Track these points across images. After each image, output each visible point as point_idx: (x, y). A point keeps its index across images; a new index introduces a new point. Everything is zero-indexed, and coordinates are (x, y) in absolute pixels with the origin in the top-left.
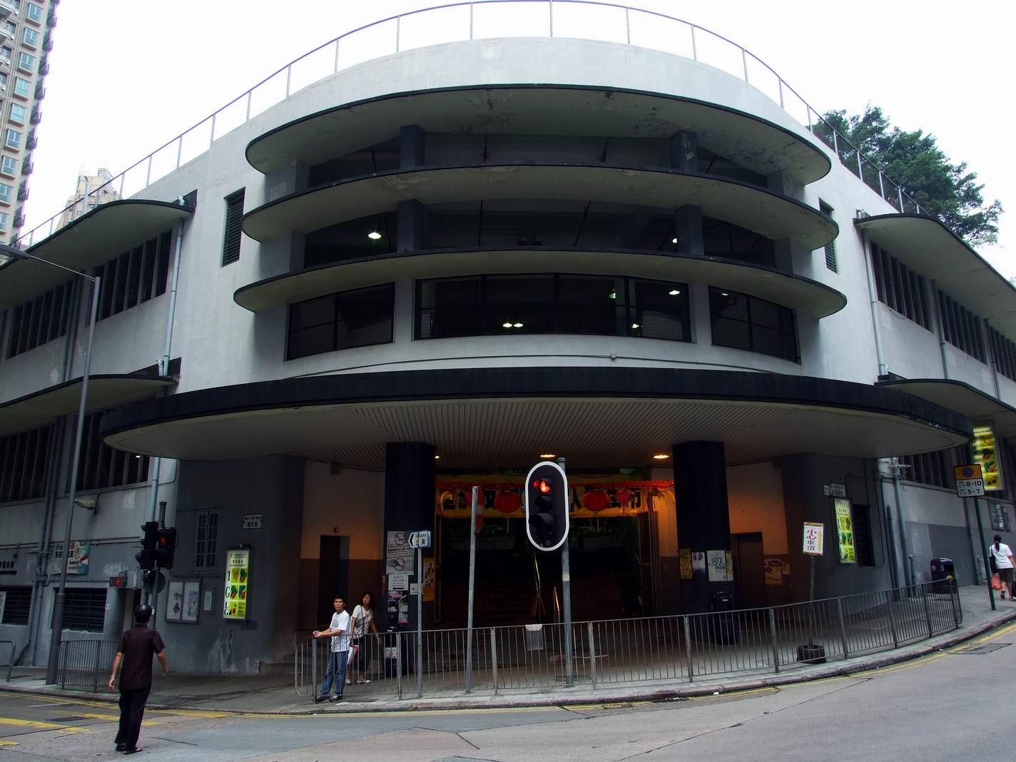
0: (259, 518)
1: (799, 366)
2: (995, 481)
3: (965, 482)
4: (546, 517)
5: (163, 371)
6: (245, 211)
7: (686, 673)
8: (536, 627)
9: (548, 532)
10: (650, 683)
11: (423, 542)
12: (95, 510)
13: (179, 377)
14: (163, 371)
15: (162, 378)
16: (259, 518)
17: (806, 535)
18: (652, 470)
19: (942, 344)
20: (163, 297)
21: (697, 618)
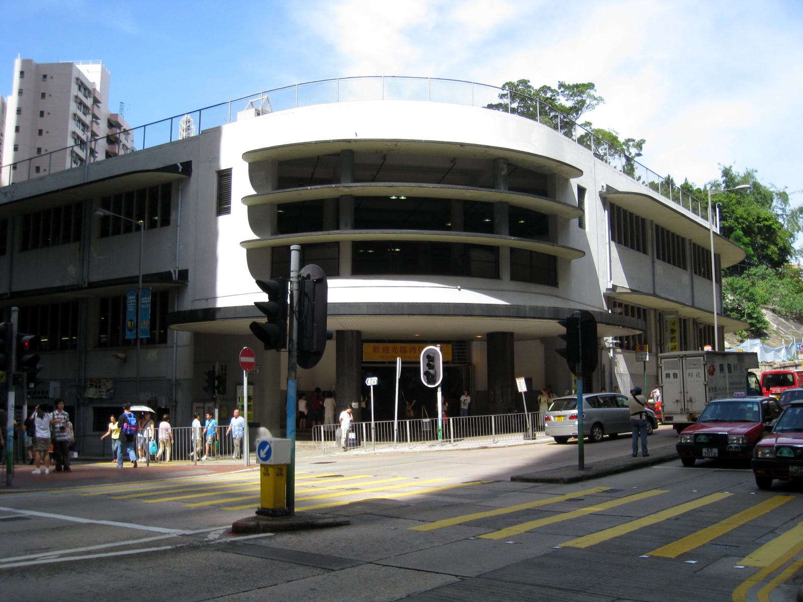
0: (258, 368)
1: (557, 289)
2: (675, 348)
3: (640, 353)
4: (431, 371)
5: (175, 277)
6: (568, 441)
7: (492, 440)
8: (428, 420)
9: (431, 379)
10: (475, 444)
11: (374, 382)
12: (125, 360)
13: (188, 282)
14: (175, 277)
15: (175, 282)
16: (258, 368)
17: (518, 384)
18: (473, 342)
19: (653, 262)
20: (168, 230)
21: (498, 417)
